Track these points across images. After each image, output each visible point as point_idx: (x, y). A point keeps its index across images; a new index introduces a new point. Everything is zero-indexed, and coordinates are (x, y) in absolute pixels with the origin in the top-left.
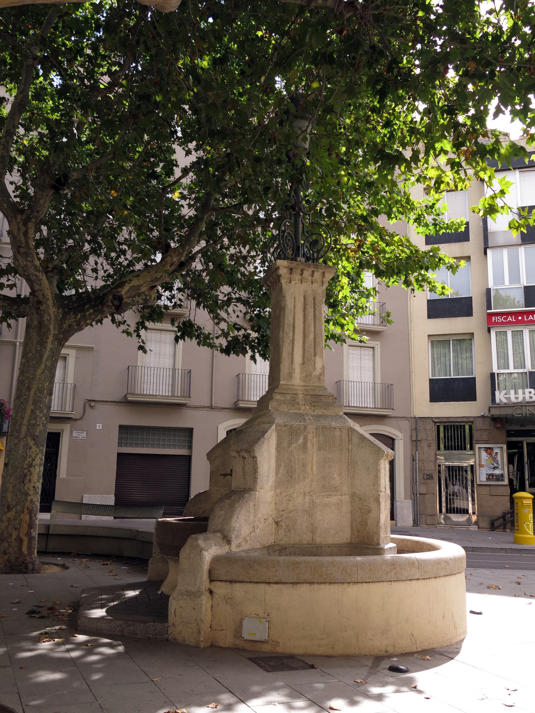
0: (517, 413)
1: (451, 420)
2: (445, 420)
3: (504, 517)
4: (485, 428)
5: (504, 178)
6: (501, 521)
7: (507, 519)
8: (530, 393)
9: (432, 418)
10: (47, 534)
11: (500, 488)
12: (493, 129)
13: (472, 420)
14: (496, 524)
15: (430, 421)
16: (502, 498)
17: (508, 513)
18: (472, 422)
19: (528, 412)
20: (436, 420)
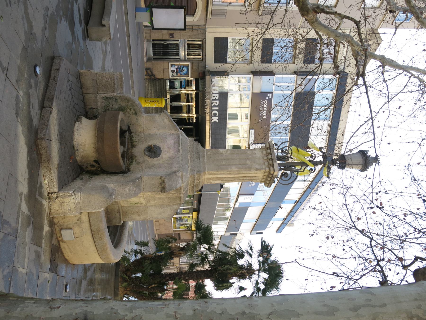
0: (207, 88)
1: (204, 49)
2: (204, 46)
3: (153, 75)
4: (199, 68)
5: (179, 305)
6: (151, 74)
7: (152, 77)
8: (217, 96)
9: (205, 38)
10: (146, 108)
11: (168, 74)
12: (381, 45)
13: (204, 61)
14: (148, 71)
15: (204, 38)
16: (162, 74)
17: (155, 78)
18: (202, 61)
19: (206, 95)
20: (204, 41)
